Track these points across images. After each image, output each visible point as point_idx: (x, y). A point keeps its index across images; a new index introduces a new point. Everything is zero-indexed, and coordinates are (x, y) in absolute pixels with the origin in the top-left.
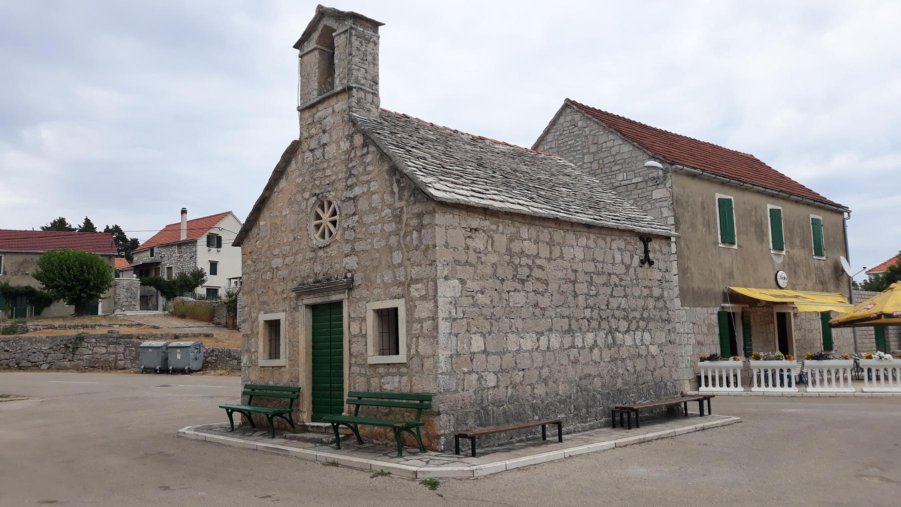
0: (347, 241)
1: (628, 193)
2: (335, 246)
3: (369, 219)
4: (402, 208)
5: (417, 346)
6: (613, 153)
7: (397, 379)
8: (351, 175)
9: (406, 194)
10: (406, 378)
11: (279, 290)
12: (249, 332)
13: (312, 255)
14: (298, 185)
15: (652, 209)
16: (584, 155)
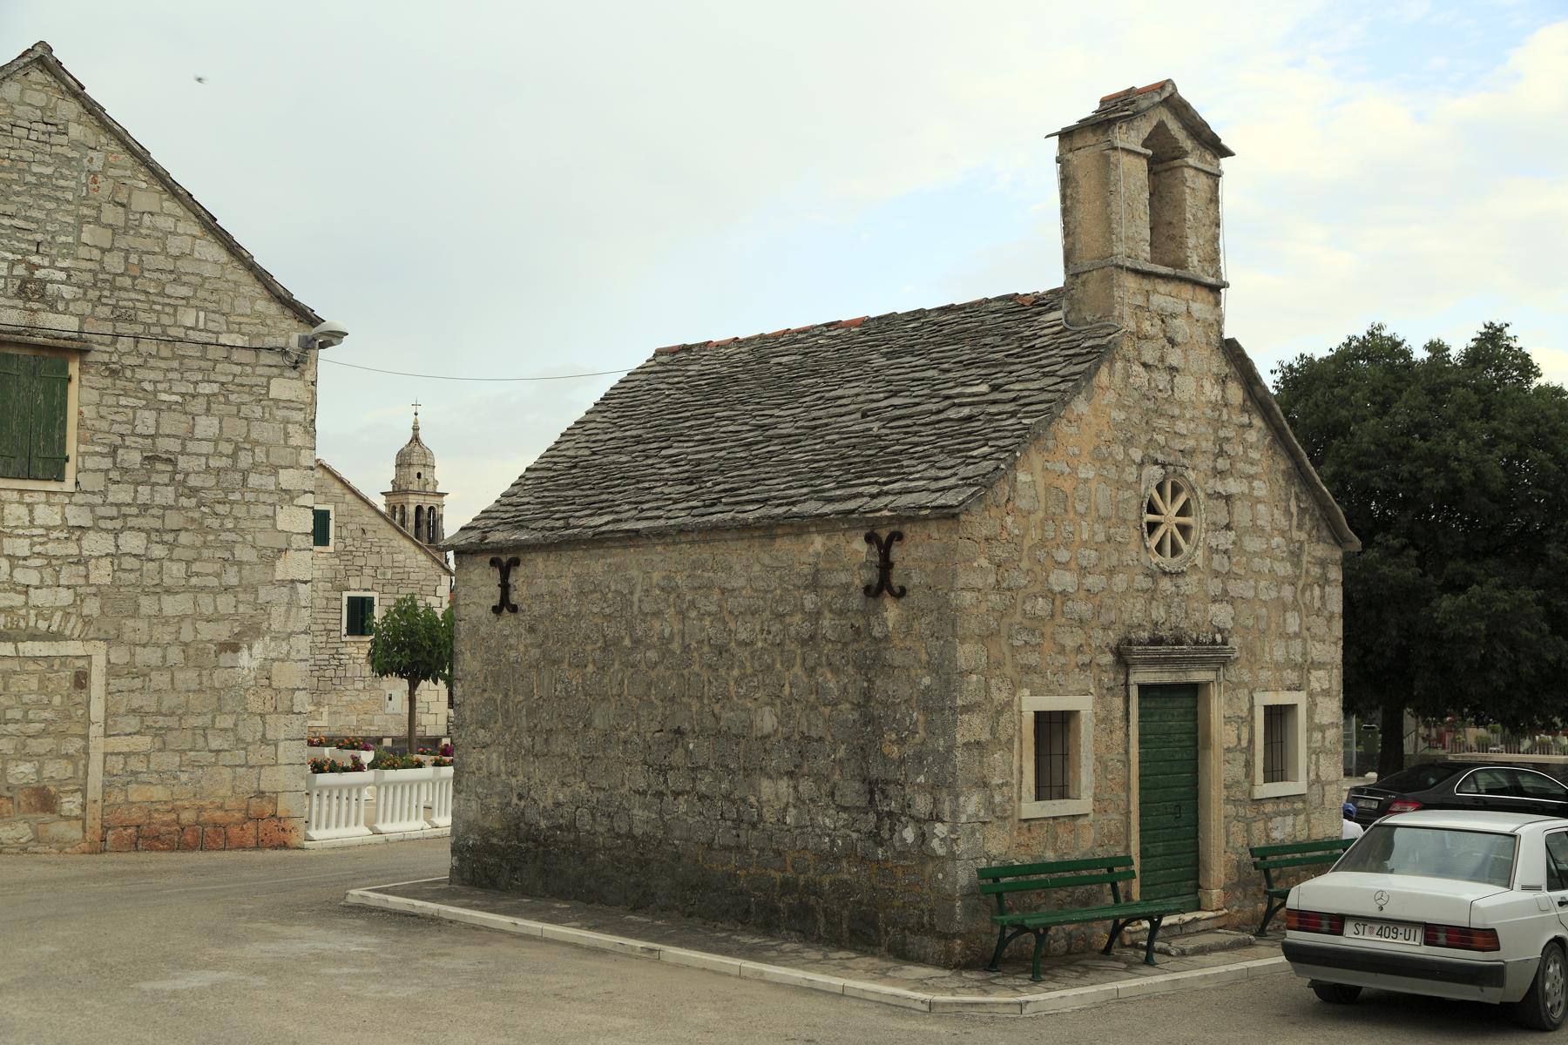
0: (1217, 574)
1: (203, 364)
2: (1193, 579)
3: (1253, 544)
4: (1302, 543)
5: (1318, 768)
6: (173, 251)
7: (1289, 820)
8: (1221, 453)
10: (1302, 817)
11: (1070, 643)
13: (1146, 583)
14: (1117, 425)
15: (262, 419)
16: (82, 220)
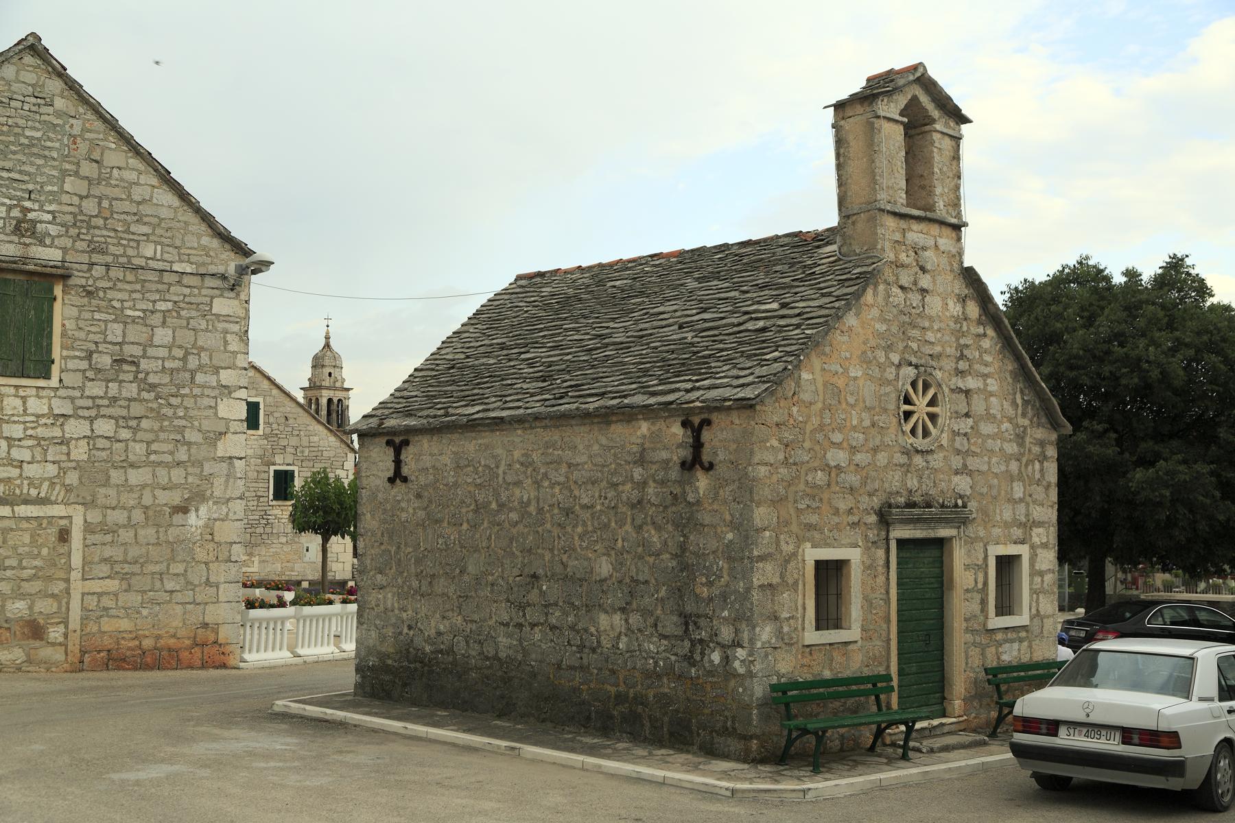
0: (958, 452)
1: (160, 287)
2: (939, 456)
3: (987, 428)
4: (1025, 428)
6: (137, 198)
7: (1016, 645)
8: (962, 357)
9: (1030, 413)
10: (1026, 644)
11: (843, 506)
12: (776, 580)
13: (903, 459)
15: (207, 330)
16: (64, 174)
